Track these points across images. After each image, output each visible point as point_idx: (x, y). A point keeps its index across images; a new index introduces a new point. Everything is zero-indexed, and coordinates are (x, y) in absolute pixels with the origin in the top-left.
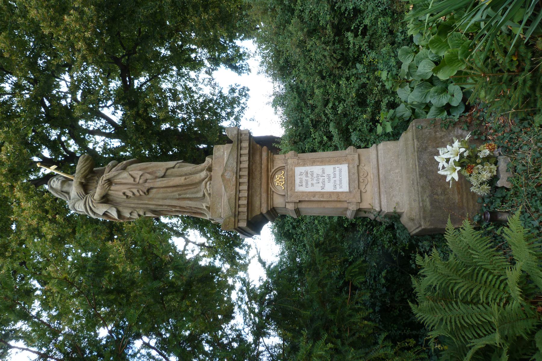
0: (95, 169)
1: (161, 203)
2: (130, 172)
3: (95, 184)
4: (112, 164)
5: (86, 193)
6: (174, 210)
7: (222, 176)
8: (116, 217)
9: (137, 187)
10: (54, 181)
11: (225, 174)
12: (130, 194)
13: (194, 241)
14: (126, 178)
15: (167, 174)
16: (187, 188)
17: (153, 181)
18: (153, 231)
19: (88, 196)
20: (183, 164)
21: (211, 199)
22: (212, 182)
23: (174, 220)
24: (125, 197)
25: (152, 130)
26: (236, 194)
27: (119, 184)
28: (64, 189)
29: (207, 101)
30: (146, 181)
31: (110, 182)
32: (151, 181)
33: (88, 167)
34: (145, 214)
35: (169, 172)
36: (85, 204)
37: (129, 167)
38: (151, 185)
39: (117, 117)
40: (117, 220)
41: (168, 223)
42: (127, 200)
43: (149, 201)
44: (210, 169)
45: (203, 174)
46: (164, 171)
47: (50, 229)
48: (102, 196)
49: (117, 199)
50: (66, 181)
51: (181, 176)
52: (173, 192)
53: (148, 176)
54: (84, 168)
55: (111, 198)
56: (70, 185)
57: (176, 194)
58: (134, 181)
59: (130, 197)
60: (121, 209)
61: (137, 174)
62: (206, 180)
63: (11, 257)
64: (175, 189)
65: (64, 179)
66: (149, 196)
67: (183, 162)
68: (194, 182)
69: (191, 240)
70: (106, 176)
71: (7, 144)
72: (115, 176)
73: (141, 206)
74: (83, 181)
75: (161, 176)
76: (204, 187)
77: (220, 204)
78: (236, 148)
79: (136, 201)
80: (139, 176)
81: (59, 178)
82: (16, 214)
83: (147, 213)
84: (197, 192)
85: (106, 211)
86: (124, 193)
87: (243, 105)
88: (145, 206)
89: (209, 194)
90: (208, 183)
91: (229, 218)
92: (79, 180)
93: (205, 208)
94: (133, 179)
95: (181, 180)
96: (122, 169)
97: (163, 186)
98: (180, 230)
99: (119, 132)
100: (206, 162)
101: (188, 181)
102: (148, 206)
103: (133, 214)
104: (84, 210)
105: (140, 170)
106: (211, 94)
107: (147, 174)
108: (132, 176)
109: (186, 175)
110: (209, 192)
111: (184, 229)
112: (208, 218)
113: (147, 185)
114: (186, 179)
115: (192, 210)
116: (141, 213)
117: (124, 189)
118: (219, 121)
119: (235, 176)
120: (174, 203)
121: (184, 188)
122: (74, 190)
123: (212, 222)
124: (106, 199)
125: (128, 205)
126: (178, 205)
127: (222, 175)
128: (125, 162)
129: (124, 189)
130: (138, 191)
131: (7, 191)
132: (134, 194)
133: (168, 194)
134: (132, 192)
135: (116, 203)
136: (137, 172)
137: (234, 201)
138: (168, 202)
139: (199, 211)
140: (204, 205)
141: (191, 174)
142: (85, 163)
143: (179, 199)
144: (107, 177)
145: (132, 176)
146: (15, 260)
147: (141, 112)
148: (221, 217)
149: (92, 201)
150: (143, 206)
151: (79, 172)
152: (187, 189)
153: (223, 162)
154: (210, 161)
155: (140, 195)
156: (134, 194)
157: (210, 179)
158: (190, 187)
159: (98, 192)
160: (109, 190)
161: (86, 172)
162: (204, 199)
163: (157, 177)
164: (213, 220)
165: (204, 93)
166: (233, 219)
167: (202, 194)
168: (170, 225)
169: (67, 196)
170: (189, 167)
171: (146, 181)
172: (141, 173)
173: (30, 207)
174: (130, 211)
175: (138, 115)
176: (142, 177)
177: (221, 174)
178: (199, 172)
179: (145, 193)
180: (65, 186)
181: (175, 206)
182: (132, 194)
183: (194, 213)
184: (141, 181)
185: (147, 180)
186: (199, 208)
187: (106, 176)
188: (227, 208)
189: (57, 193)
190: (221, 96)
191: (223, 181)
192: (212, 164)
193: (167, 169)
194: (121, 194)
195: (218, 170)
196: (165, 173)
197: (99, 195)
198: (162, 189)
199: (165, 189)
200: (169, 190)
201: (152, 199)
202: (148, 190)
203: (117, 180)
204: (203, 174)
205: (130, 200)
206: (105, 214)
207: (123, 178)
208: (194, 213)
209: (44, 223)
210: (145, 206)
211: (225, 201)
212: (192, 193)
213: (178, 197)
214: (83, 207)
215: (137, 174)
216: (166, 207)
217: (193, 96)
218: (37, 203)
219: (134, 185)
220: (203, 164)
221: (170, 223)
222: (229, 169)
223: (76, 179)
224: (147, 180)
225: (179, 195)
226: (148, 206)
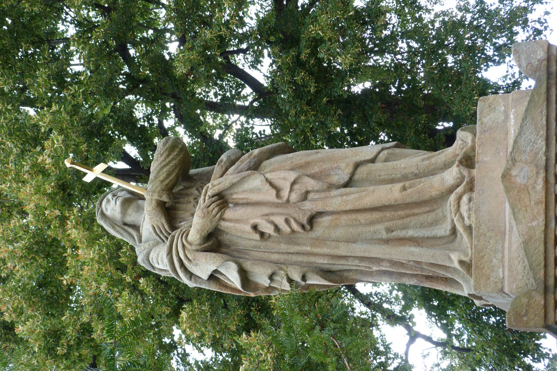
0: (193, 171)
1: (343, 250)
2: (268, 176)
3: (190, 206)
4: (229, 157)
5: (173, 228)
6: (375, 268)
7: (504, 176)
8: (239, 287)
9: (285, 211)
10: (108, 201)
11: (514, 172)
12: (269, 229)
13: (428, 335)
14: (257, 190)
15: (356, 177)
16: (408, 212)
17: (323, 195)
18: (318, 328)
19: (177, 233)
20: (398, 150)
21: (475, 242)
22: (474, 195)
23: (384, 288)
24: (257, 237)
25: (330, 96)
26: (547, 226)
27: (243, 204)
28: (129, 219)
29: (453, 26)
30: (305, 196)
31: (222, 200)
32: (317, 196)
33: (176, 166)
34: (304, 278)
35: (362, 171)
36: (170, 252)
37: (266, 163)
38: (319, 207)
39: (263, 72)
40: (239, 291)
41: (371, 294)
42: (263, 244)
43: (313, 245)
44: (468, 161)
45: (451, 175)
46: (350, 170)
47: (130, 305)
48: (205, 233)
49: (239, 241)
50: (133, 199)
51: (392, 181)
52: (372, 223)
53: (310, 184)
54: (165, 170)
55: (225, 238)
56: (140, 209)
57: (381, 227)
58: (278, 196)
59: (270, 236)
60: (248, 265)
61: (284, 179)
62: (460, 189)
63: (67, 356)
64: (376, 215)
65: (129, 196)
66: (312, 234)
67: (396, 146)
68: (427, 197)
69: (422, 332)
70: (214, 186)
71: (54, 135)
72: (233, 185)
73: (295, 258)
74: (165, 198)
75: (342, 182)
76: (453, 209)
77: (499, 256)
78: (543, 97)
79: (284, 247)
80: (288, 185)
81: (119, 194)
82: (71, 272)
83: (309, 275)
84: (435, 223)
85: (216, 271)
86: (255, 227)
87: (538, 26)
88: (305, 259)
89: (469, 229)
90: (465, 198)
91: (528, 295)
92: (156, 197)
93: (456, 265)
94: (274, 192)
95: (392, 193)
96: (249, 169)
97: (348, 208)
98: (397, 309)
99: (266, 102)
100: (457, 143)
101: (412, 195)
102: (312, 259)
103: (276, 278)
104: (168, 268)
105: (292, 169)
106: (460, 9)
107: (307, 179)
108: (271, 184)
109: (405, 178)
110: (467, 222)
111: (406, 308)
112: (465, 293)
113: (309, 207)
114: (404, 189)
115: (422, 269)
116: (297, 278)
117: (255, 216)
118: (478, 66)
119: (542, 175)
120: (377, 251)
121: (401, 213)
122: (148, 220)
123: (477, 303)
124: (214, 242)
125: (266, 256)
126: (387, 257)
127: (506, 176)
128: (256, 151)
129: (255, 216)
130: (287, 221)
131: (55, 227)
132: (277, 229)
133: (360, 229)
134: (272, 223)
135: (239, 251)
136: (283, 174)
137: (542, 248)
138: (359, 249)
139: (442, 273)
140: (455, 257)
141: (417, 176)
142: (168, 156)
143: (387, 241)
144: (216, 190)
145: (271, 184)
146: (74, 362)
147: (303, 57)
148: (502, 291)
149: (183, 246)
150: (300, 259)
151: (156, 178)
152: (408, 216)
153: (506, 139)
154: (469, 141)
155: (293, 231)
156: (277, 229)
157: (471, 188)
158: (416, 211)
159: (196, 224)
160: (222, 219)
161: (171, 178)
162: (453, 241)
163: (331, 186)
164: (480, 298)
165: (444, 8)
166: (539, 299)
167: (449, 227)
168: (374, 299)
169: (134, 233)
170: (414, 159)
171: (305, 196)
172: (292, 176)
173: (92, 260)
174: (270, 272)
175: (299, 63)
176: (296, 187)
177: (499, 172)
178: (439, 170)
179: (303, 227)
180: (130, 211)
181: (378, 261)
182: (272, 228)
183: (429, 278)
184: (294, 197)
185: (307, 192)
186: (440, 266)
187: (214, 186)
188: (520, 268)
189: (113, 228)
190: (482, 12)
191: (508, 190)
192: (473, 148)
193: (357, 165)
194: (248, 228)
195: (491, 165)
196: (353, 174)
197: (198, 231)
198: (344, 217)
199: (354, 216)
200: (362, 217)
201: (320, 241)
202: (312, 220)
203: (238, 195)
204: (451, 175)
205: (269, 244)
206: (213, 277)
207: (252, 191)
208: (429, 278)
209: (119, 292)
210: (305, 259)
211: (515, 246)
212: (422, 226)
213: (384, 235)
214: (166, 261)
215: (283, 179)
216: (356, 262)
217: (420, 19)
218: (104, 250)
219: (277, 205)
220: (449, 151)
221: (376, 294)
222: (524, 157)
223: (150, 192)
224: (307, 192)
225: (389, 230)
226: (312, 259)
